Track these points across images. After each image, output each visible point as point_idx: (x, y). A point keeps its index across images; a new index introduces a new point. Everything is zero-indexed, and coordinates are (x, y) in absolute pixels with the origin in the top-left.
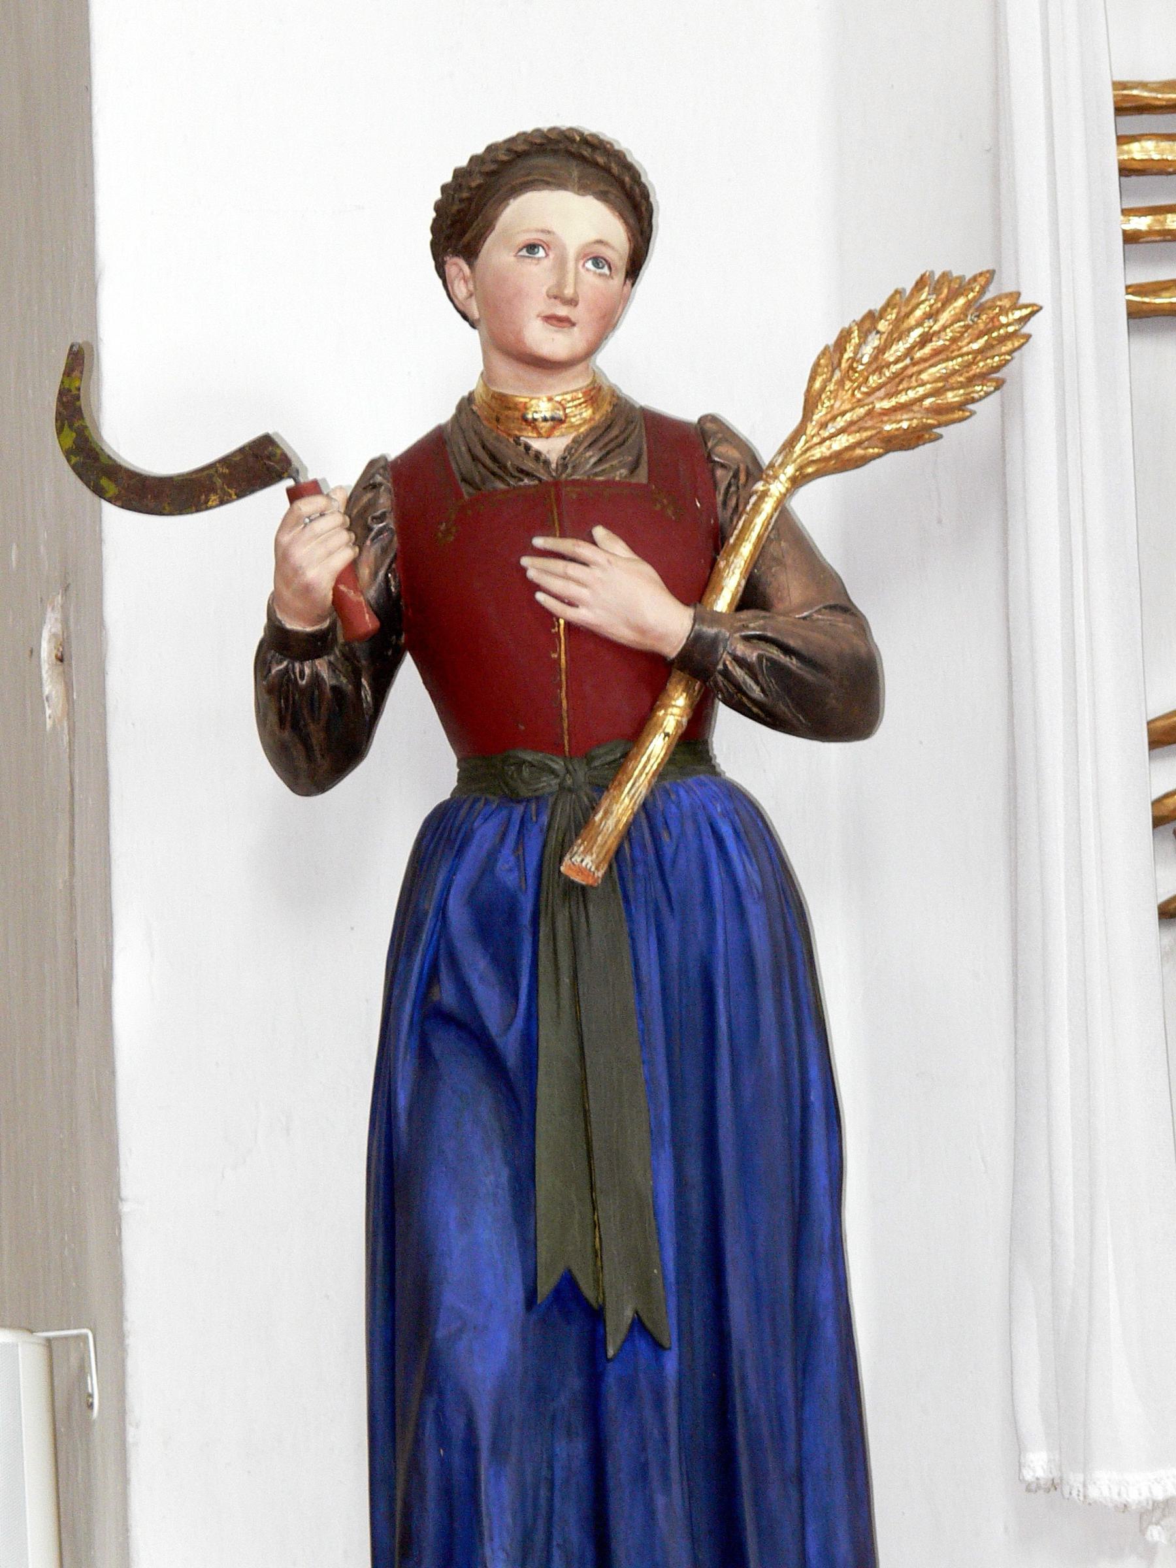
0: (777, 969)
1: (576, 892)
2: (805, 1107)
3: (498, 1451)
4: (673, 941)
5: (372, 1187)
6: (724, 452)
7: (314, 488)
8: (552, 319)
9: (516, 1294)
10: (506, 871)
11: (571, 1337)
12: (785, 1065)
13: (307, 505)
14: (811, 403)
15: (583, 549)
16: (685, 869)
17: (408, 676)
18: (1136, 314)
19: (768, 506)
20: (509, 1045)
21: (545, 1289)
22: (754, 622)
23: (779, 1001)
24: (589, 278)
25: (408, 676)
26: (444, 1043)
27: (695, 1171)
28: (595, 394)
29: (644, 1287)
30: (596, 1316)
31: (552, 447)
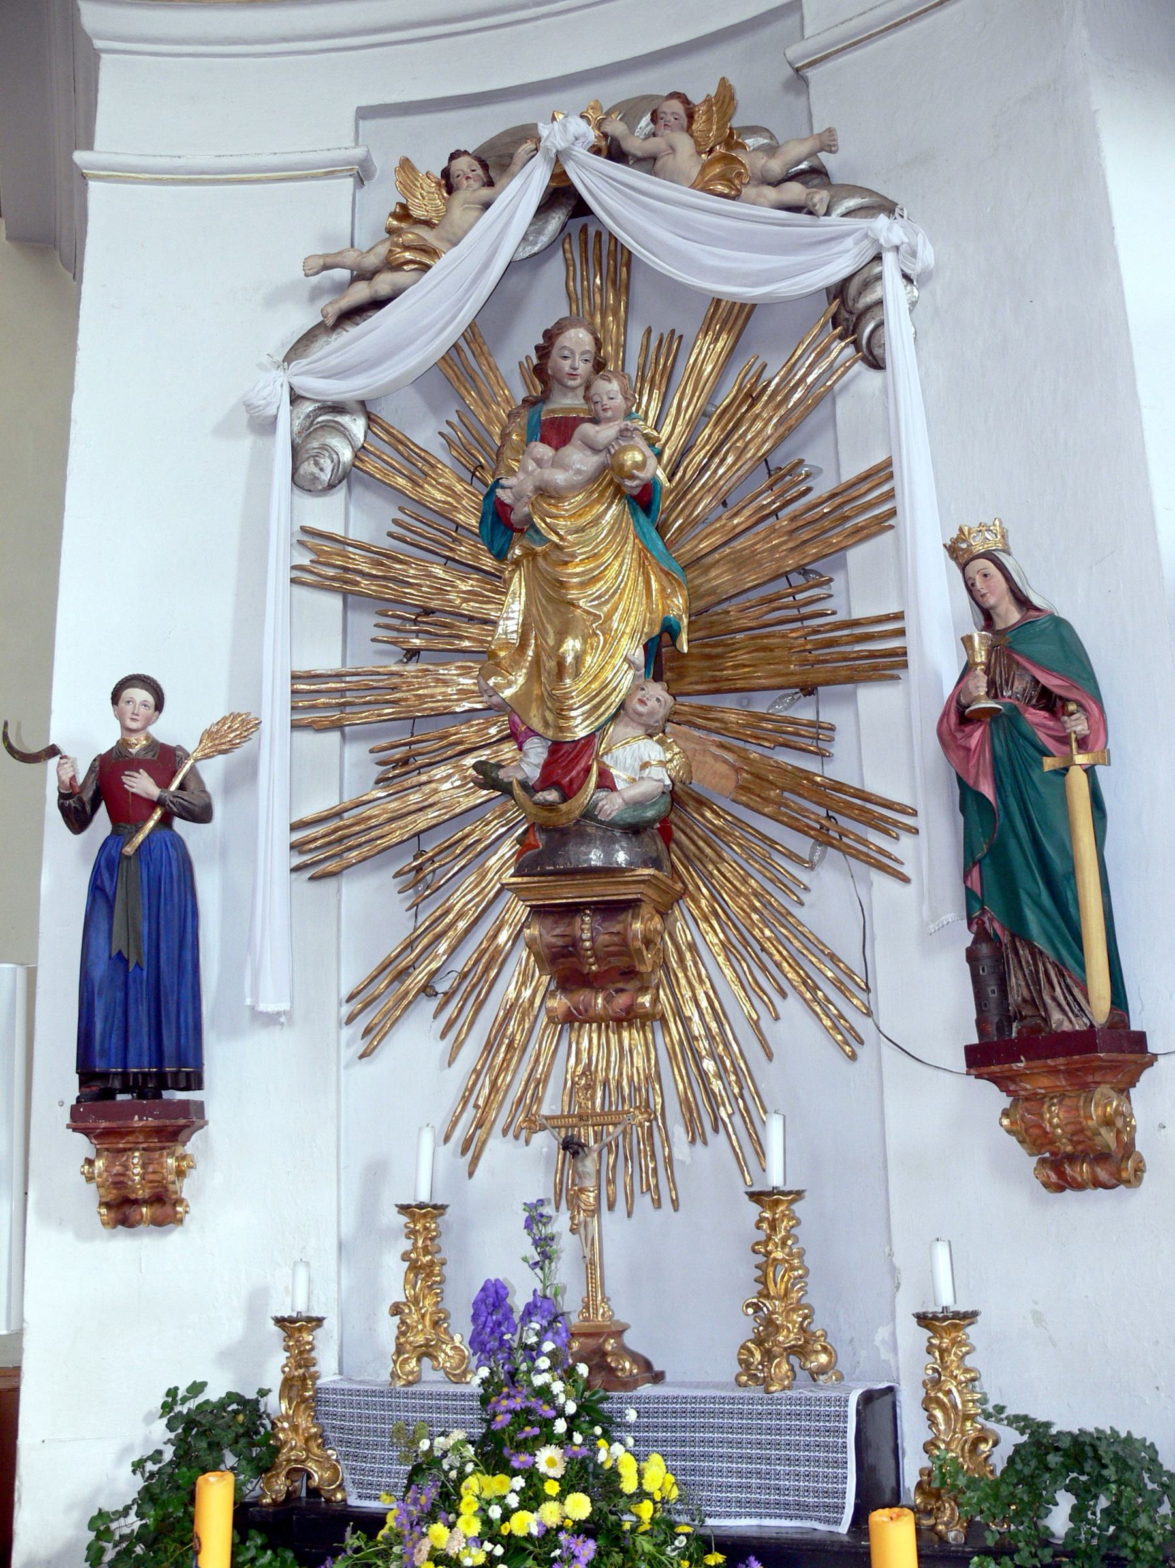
0: (179, 876)
1: (128, 858)
2: (186, 911)
3: (100, 994)
4: (152, 869)
5: (190, 967)
6: (179, 753)
7: (65, 757)
8: (132, 719)
9: (107, 955)
10: (113, 852)
11: (122, 965)
12: (180, 901)
13: (64, 760)
14: (201, 742)
15: (136, 774)
16: (156, 854)
17: (103, 808)
18: (292, 727)
19: (187, 767)
20: (110, 894)
21: (114, 953)
22: (182, 794)
23: (179, 886)
24: (143, 710)
25: (103, 808)
26: (98, 892)
27: (154, 927)
28: (148, 738)
29: (139, 954)
30: (127, 962)
31: (133, 751)
